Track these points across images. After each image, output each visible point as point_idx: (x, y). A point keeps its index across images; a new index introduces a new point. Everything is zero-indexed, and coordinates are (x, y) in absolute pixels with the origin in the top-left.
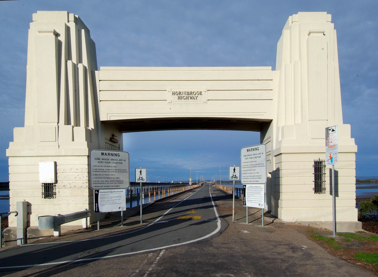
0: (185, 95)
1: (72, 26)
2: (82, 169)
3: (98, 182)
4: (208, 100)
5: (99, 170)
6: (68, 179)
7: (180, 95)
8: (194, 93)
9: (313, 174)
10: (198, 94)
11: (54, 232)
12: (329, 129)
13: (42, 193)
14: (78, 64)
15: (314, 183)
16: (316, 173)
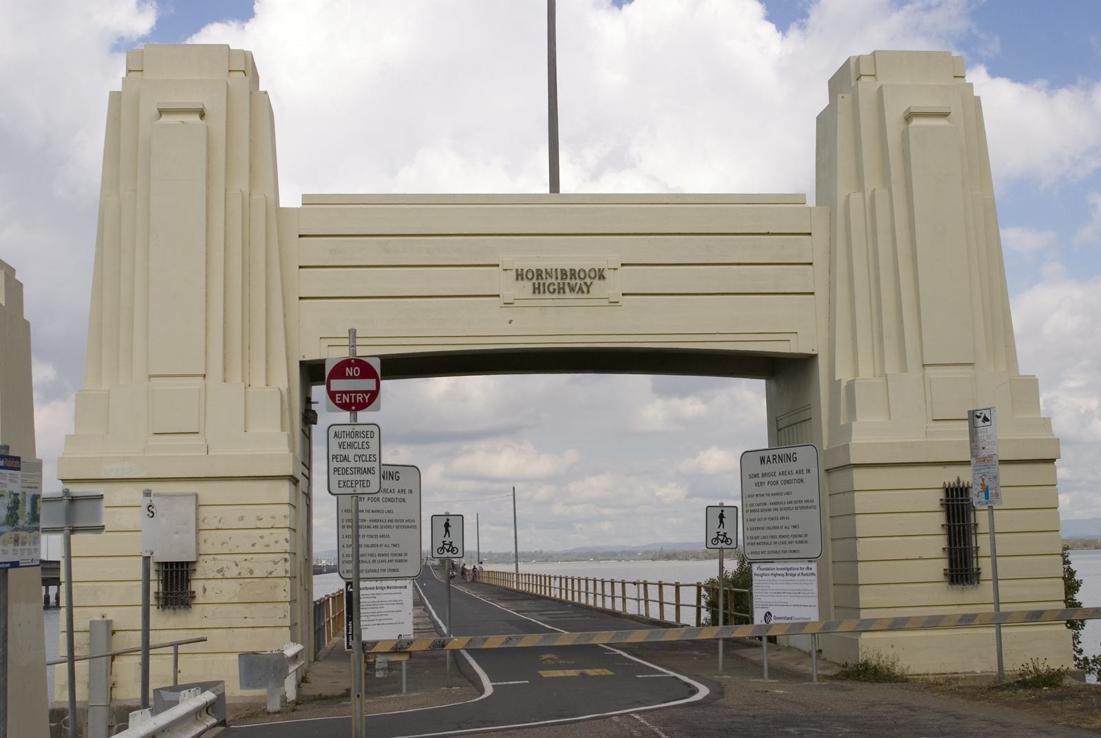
0: (553, 280)
6: (231, 550)
7: (542, 282)
12: (977, 416)
16: (952, 523)
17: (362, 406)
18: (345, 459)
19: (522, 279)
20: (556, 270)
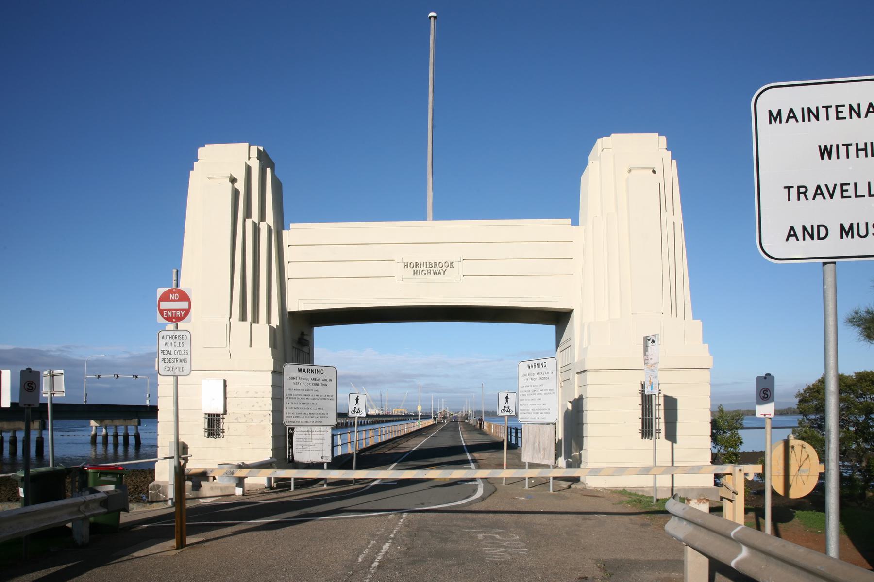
1: (255, 164)
2: (263, 392)
3: (293, 415)
4: (463, 276)
5: (295, 397)
7: (417, 269)
8: (441, 265)
9: (640, 405)
10: (447, 265)
11: (237, 488)
13: (204, 430)
14: (259, 223)
15: (640, 420)
17: (181, 319)
18: (169, 353)
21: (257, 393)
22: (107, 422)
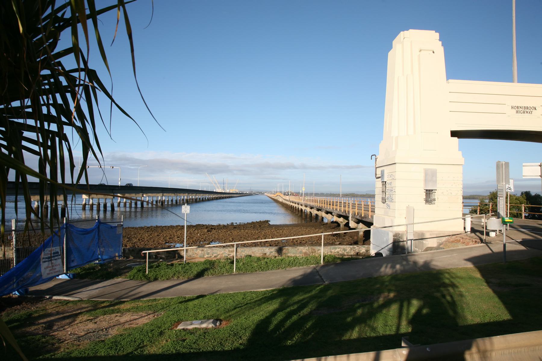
0: (522, 110)
7: (518, 110)
19: (517, 106)
20: (523, 107)
21: (454, 178)
22: (93, 196)
